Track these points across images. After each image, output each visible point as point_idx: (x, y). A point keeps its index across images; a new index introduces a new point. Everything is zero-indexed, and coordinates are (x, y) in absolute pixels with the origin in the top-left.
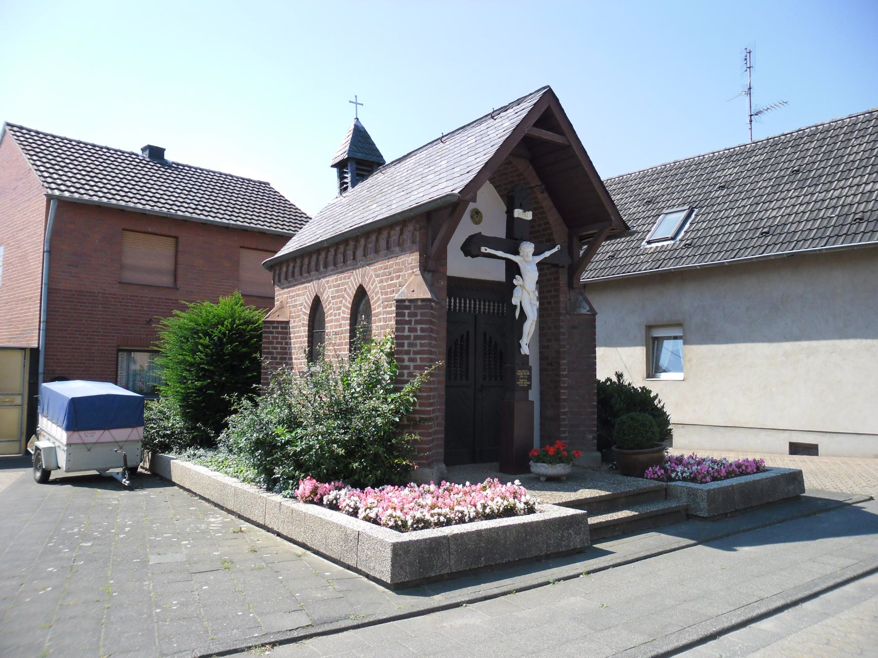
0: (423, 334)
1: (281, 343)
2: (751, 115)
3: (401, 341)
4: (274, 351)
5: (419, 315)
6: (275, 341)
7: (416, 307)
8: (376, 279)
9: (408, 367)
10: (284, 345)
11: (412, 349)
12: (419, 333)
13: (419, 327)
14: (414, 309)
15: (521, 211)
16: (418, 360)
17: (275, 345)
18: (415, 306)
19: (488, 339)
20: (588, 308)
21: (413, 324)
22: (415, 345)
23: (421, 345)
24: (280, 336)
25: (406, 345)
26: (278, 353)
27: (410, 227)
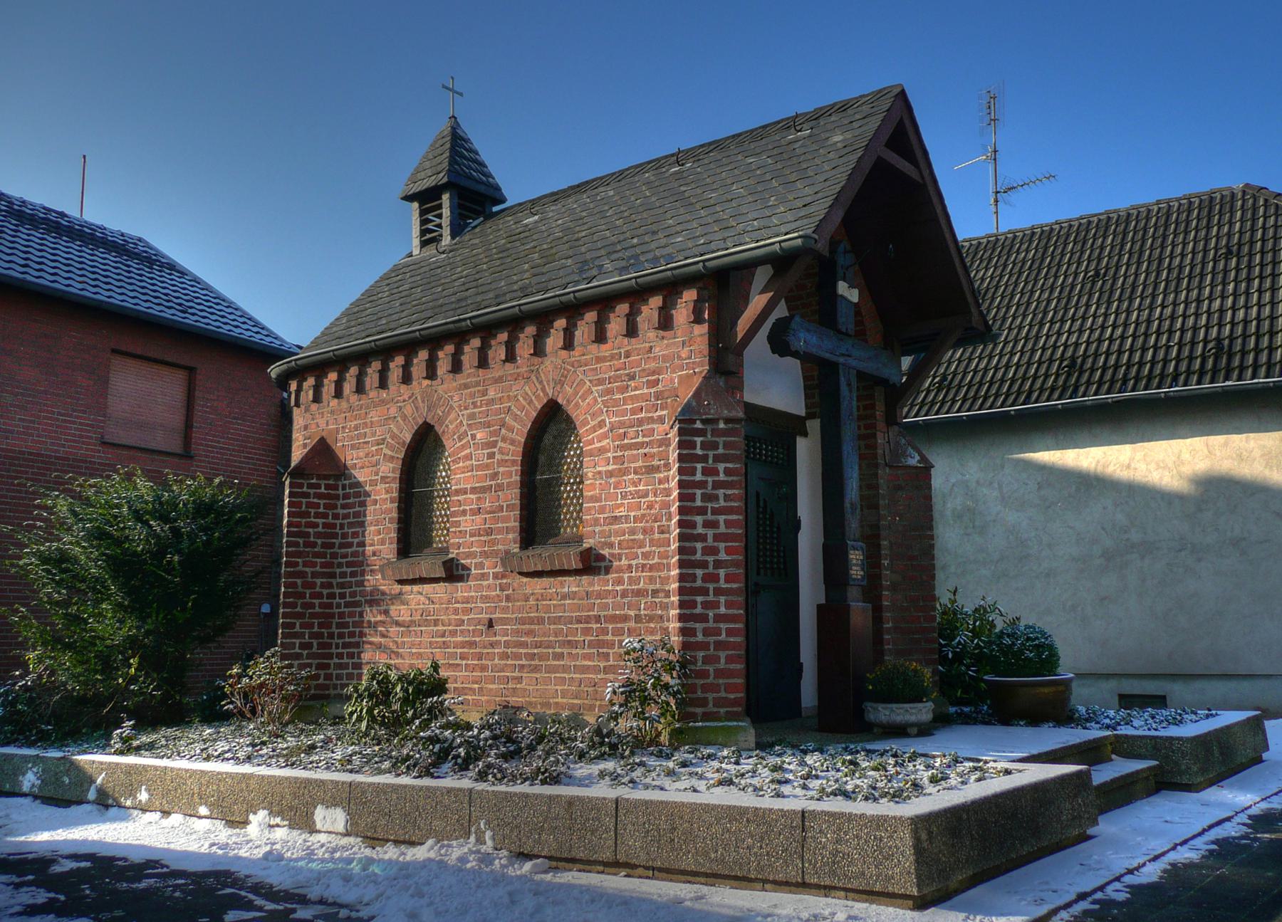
0: (730, 479)
1: (325, 516)
2: (997, 192)
3: (690, 491)
4: (311, 530)
5: (721, 446)
6: (313, 511)
7: (716, 432)
8: (594, 389)
9: (702, 538)
10: (330, 520)
11: (710, 505)
12: (722, 477)
13: (721, 467)
14: (712, 436)
15: (846, 285)
16: (722, 523)
17: (312, 519)
18: (713, 430)
19: (762, 504)
20: (917, 458)
21: (710, 461)
22: (716, 498)
23: (727, 498)
24: (322, 502)
25: (698, 497)
26: (318, 535)
27: (690, 295)
